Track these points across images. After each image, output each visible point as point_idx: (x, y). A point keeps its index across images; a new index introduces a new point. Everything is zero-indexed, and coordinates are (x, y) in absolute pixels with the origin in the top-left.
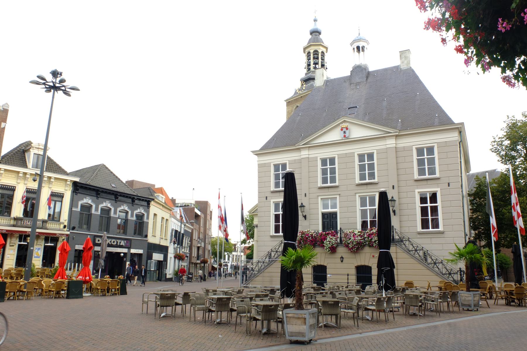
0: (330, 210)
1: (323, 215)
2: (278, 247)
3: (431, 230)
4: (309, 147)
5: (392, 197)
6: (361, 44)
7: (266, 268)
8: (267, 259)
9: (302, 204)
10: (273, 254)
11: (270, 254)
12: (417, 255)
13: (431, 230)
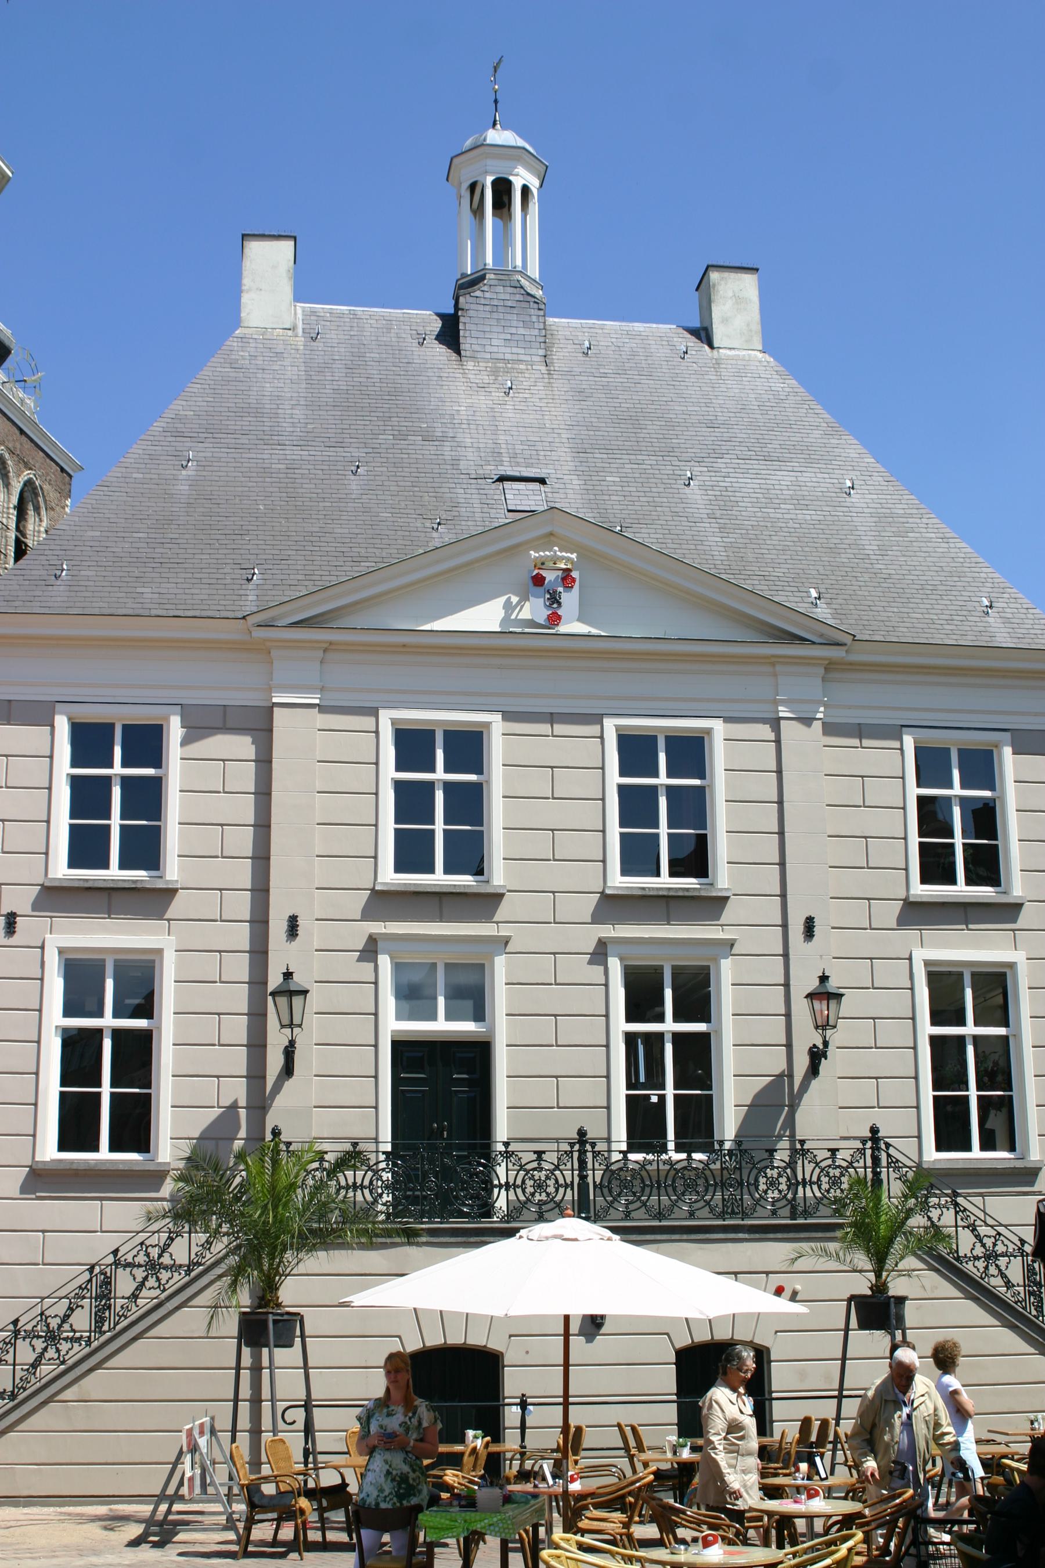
0: (442, 1025)
1: (406, 1052)
2: (62, 1308)
3: (104, 1154)
4: (329, 648)
5: (824, 979)
6: (37, 390)
7: (71, 1373)
8: (82, 1320)
9: (288, 975)
10: (124, 1283)
11: (107, 1282)
12: (997, 1281)
13: (104, 1154)
